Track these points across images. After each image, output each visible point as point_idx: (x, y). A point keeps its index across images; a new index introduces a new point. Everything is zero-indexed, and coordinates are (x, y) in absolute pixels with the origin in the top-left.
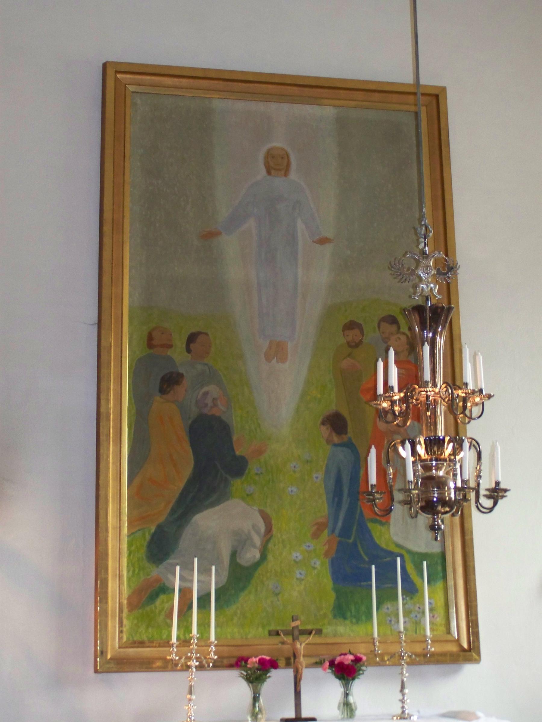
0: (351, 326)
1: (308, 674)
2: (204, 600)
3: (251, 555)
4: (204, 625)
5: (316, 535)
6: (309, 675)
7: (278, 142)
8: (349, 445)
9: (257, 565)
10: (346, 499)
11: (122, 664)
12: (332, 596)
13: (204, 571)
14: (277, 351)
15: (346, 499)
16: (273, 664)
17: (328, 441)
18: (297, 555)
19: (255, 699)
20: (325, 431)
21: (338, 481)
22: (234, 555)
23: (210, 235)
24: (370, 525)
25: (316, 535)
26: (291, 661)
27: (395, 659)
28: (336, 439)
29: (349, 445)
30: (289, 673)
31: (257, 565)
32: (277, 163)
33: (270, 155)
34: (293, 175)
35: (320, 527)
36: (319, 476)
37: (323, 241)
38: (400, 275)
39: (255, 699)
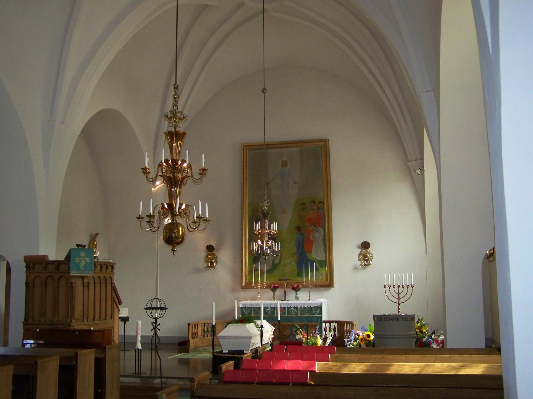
0: (303, 204)
1: (287, 290)
2: (262, 273)
3: (277, 261)
4: (312, 276)
5: (293, 256)
6: (287, 290)
7: (285, 158)
8: (302, 234)
9: (278, 264)
10: (301, 247)
11: (248, 286)
12: (297, 271)
13: (262, 265)
14: (284, 212)
15: (301, 247)
16: (277, 287)
17: (296, 233)
18: (288, 261)
19: (274, 295)
20: (296, 231)
21: (299, 243)
22: (273, 261)
23: (268, 184)
24: (307, 254)
25: (293, 256)
26: (282, 286)
27: (307, 287)
28: (298, 233)
29: (302, 234)
30: (283, 290)
31: (278, 264)
32: (284, 164)
33: (282, 162)
34: (288, 167)
35: (294, 254)
36: (294, 242)
37: (296, 183)
38: (107, 267)
39: (274, 295)
